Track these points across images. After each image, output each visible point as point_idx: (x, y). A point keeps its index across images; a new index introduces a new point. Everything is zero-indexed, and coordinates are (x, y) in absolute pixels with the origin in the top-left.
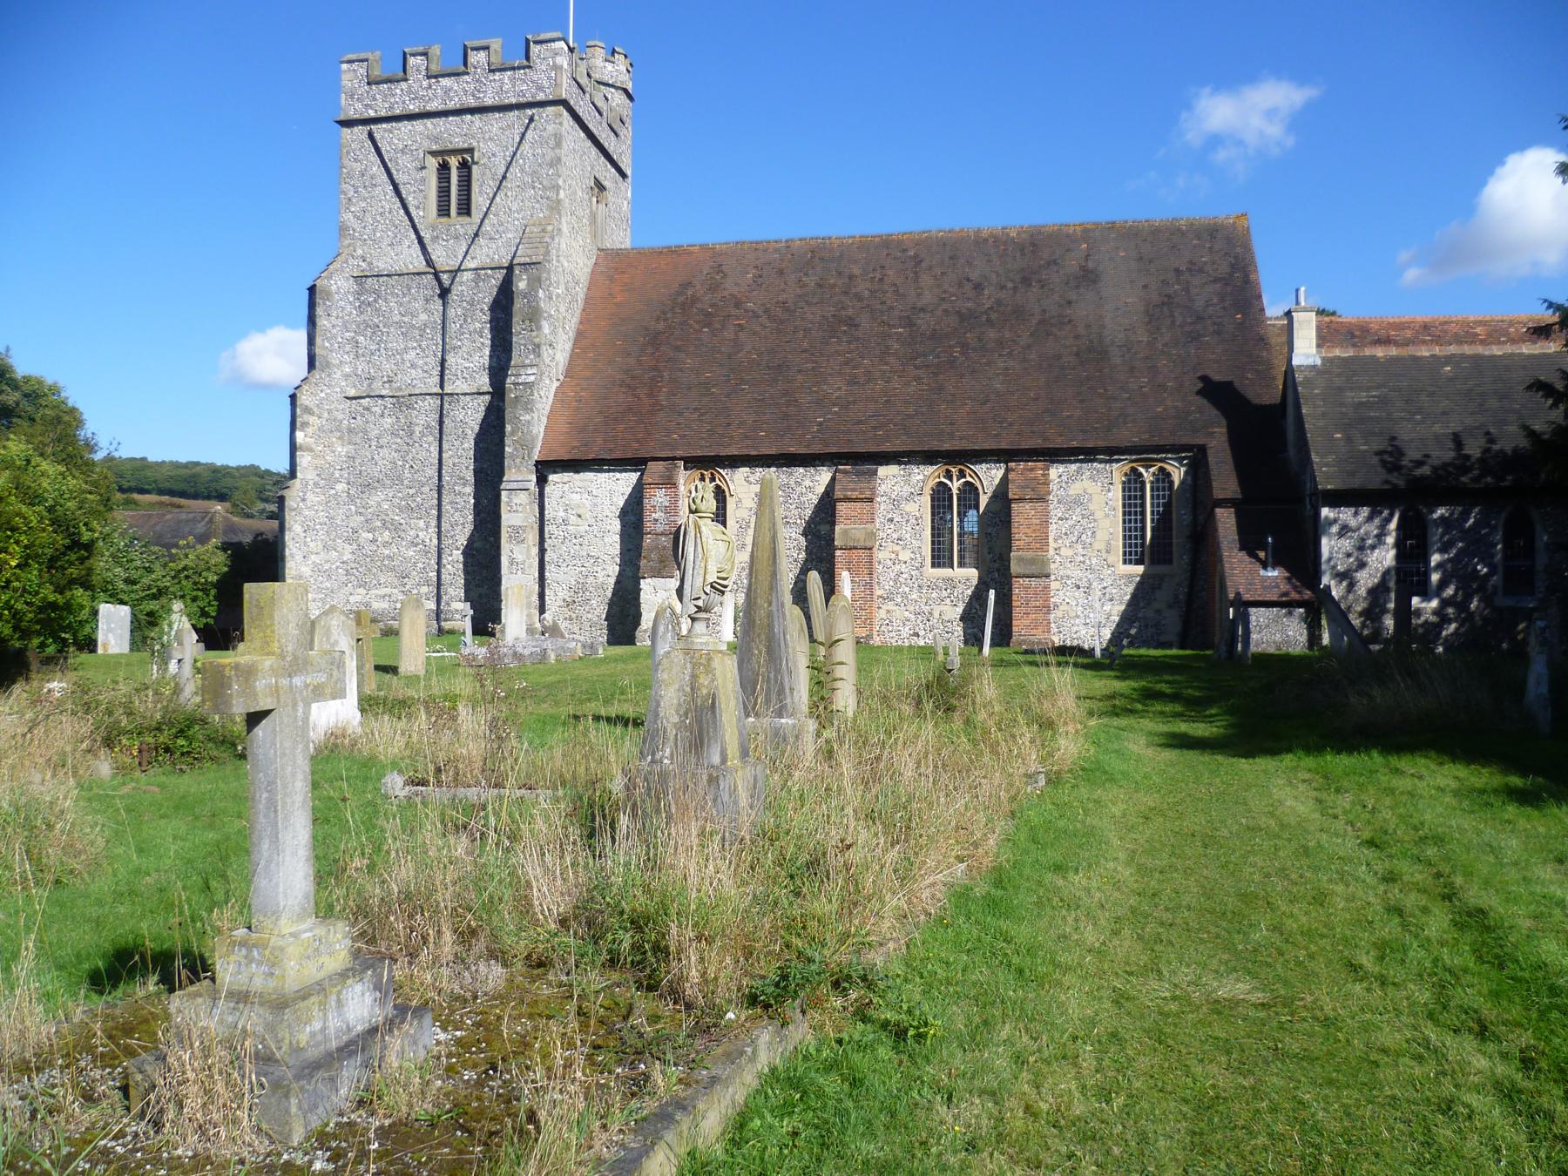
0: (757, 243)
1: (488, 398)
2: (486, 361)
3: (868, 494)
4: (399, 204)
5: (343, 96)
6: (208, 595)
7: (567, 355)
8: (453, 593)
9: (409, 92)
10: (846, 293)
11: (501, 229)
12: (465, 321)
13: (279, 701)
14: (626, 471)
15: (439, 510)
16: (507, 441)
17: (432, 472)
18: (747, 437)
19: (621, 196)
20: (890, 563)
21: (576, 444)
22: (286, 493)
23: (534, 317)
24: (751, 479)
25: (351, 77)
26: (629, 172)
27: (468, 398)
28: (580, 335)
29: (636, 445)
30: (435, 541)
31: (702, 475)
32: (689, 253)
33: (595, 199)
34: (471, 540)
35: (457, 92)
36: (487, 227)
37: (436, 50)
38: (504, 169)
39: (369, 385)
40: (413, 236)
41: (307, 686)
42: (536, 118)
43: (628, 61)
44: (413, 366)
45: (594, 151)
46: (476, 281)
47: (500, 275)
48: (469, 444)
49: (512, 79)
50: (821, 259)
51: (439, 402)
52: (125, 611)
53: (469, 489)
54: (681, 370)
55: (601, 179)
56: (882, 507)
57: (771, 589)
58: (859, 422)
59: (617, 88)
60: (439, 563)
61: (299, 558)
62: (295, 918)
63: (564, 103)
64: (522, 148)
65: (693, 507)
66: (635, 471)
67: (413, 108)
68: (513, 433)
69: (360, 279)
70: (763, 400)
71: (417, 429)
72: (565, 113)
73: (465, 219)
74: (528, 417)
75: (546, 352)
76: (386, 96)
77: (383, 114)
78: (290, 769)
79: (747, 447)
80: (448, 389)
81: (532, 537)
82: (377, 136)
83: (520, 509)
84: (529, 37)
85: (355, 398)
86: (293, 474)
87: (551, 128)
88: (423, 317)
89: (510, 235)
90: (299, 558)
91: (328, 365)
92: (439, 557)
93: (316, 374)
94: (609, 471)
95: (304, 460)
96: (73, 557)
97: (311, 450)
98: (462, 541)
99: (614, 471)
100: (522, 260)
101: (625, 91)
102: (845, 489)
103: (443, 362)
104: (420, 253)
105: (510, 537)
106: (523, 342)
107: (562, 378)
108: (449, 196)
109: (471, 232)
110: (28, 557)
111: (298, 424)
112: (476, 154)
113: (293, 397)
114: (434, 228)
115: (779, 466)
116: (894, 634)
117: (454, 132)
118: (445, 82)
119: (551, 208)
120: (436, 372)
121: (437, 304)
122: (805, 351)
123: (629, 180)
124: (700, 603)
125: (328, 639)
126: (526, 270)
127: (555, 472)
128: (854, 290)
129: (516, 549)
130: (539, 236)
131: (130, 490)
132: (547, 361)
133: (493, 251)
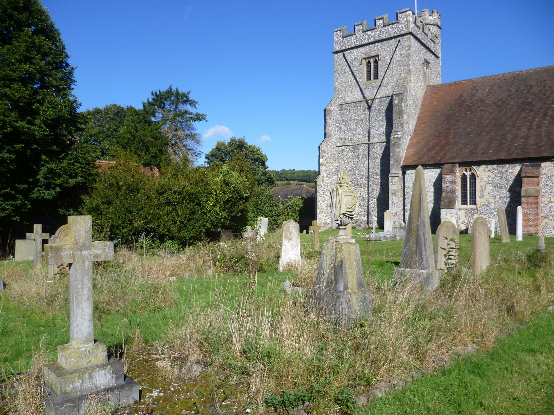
0: (490, 76)
1: (385, 144)
2: (384, 130)
3: (536, 174)
4: (353, 78)
5: (334, 43)
6: (296, 214)
7: (414, 126)
8: (373, 214)
9: (356, 38)
10: (528, 93)
11: (389, 82)
12: (377, 117)
13: (74, 260)
14: (436, 168)
15: (368, 185)
16: (391, 159)
17: (366, 171)
18: (484, 153)
19: (437, 65)
20: (547, 203)
21: (417, 159)
22: (316, 180)
23: (401, 113)
24: (486, 170)
25: (337, 36)
26: (440, 56)
27: (378, 144)
28: (419, 118)
29: (440, 158)
30: (367, 196)
31: (466, 169)
32: (463, 84)
33: (425, 67)
34: (379, 195)
35: (373, 35)
36: (384, 82)
37: (365, 22)
38: (390, 61)
39: (344, 142)
40: (358, 88)
41: (91, 255)
42: (401, 40)
43: (438, 14)
44: (359, 134)
45: (424, 50)
46: (381, 102)
47: (389, 99)
48: (379, 161)
49: (392, 28)
50: (518, 80)
51: (368, 146)
52: (266, 219)
53: (379, 177)
54: (458, 129)
55: (428, 60)
56: (543, 180)
57: (418, 215)
58: (533, 145)
59: (434, 25)
60: (368, 203)
61: (321, 202)
62: (82, 342)
63: (411, 33)
64: (396, 52)
65: (339, 182)
66: (439, 168)
67: (358, 44)
68: (393, 156)
69: (341, 105)
70: (491, 138)
71: (361, 156)
72: (412, 37)
73: (377, 80)
74: (398, 150)
75: (405, 126)
76: (348, 41)
77: (347, 47)
78: (80, 286)
79: (485, 157)
80: (371, 141)
81: (400, 194)
82: (346, 55)
83: (396, 183)
84: (398, 12)
85: (340, 146)
86: (319, 173)
87: (406, 43)
88: (362, 116)
89: (392, 84)
90: (321, 202)
91: (330, 136)
92: (368, 201)
93: (327, 139)
94: (429, 168)
95: (323, 168)
96: (241, 202)
97: (325, 165)
98: (376, 195)
99: (431, 168)
100: (396, 93)
101: (438, 26)
102: (526, 173)
103: (369, 132)
104: (361, 94)
105: (392, 194)
106: (397, 122)
107: (412, 135)
108: (371, 73)
109: (378, 85)
110: (216, 202)
111: (321, 156)
112: (380, 57)
113: (319, 147)
114: (365, 85)
115: (498, 164)
116: (548, 232)
117: (371, 50)
118: (368, 33)
119: (407, 73)
120: (367, 135)
121: (367, 112)
122: (510, 117)
123: (440, 59)
124: (339, 222)
125: (289, 231)
126: (397, 96)
127: (409, 170)
128: (532, 91)
129: (394, 198)
130: (403, 84)
131: (290, 180)
132: (406, 129)
133: (385, 91)
